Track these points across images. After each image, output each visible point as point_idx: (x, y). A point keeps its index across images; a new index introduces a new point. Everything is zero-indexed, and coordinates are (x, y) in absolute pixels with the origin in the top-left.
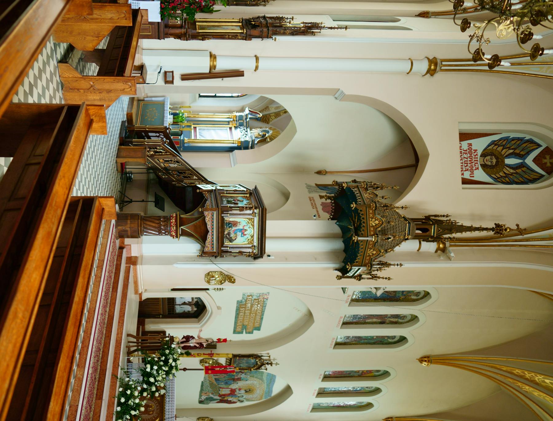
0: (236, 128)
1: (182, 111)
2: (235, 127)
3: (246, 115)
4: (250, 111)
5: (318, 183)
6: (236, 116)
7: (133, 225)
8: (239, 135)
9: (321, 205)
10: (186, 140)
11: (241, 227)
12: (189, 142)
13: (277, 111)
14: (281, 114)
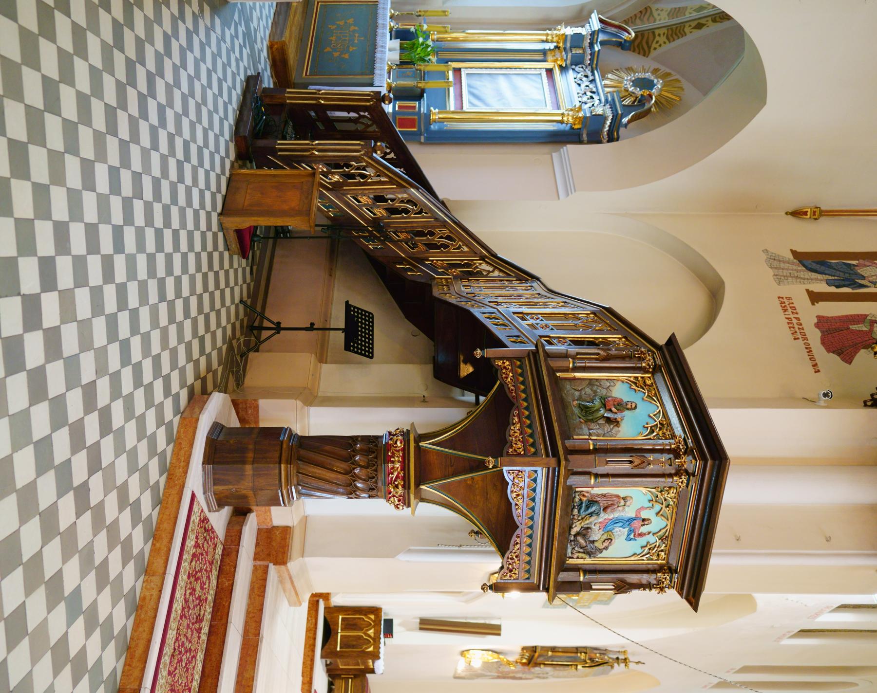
0: (563, 69)
1: (425, 27)
2: (561, 67)
3: (593, 34)
4: (601, 21)
5: (800, 249)
6: (565, 37)
7: (261, 482)
8: (574, 95)
9: (817, 325)
10: (436, 114)
11: (629, 512)
12: (441, 121)
13: (676, 21)
14: (687, 30)
